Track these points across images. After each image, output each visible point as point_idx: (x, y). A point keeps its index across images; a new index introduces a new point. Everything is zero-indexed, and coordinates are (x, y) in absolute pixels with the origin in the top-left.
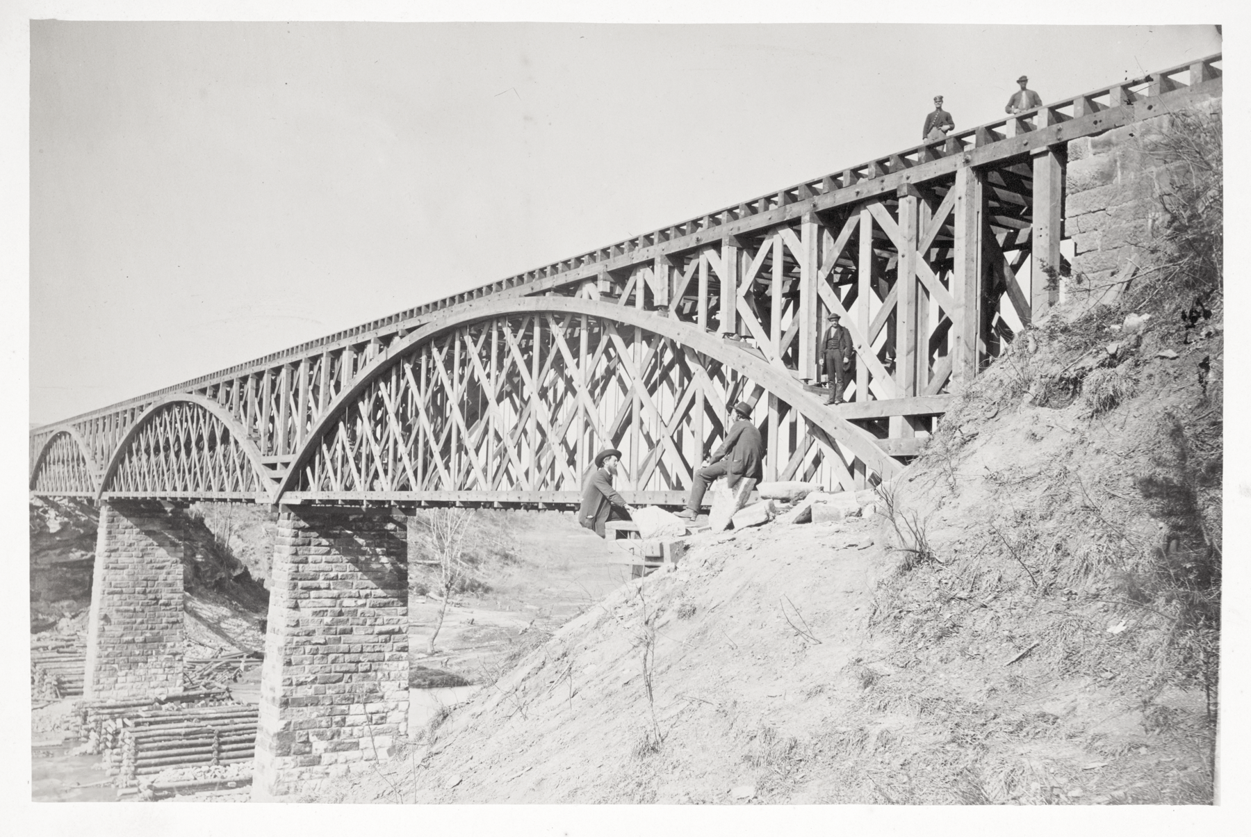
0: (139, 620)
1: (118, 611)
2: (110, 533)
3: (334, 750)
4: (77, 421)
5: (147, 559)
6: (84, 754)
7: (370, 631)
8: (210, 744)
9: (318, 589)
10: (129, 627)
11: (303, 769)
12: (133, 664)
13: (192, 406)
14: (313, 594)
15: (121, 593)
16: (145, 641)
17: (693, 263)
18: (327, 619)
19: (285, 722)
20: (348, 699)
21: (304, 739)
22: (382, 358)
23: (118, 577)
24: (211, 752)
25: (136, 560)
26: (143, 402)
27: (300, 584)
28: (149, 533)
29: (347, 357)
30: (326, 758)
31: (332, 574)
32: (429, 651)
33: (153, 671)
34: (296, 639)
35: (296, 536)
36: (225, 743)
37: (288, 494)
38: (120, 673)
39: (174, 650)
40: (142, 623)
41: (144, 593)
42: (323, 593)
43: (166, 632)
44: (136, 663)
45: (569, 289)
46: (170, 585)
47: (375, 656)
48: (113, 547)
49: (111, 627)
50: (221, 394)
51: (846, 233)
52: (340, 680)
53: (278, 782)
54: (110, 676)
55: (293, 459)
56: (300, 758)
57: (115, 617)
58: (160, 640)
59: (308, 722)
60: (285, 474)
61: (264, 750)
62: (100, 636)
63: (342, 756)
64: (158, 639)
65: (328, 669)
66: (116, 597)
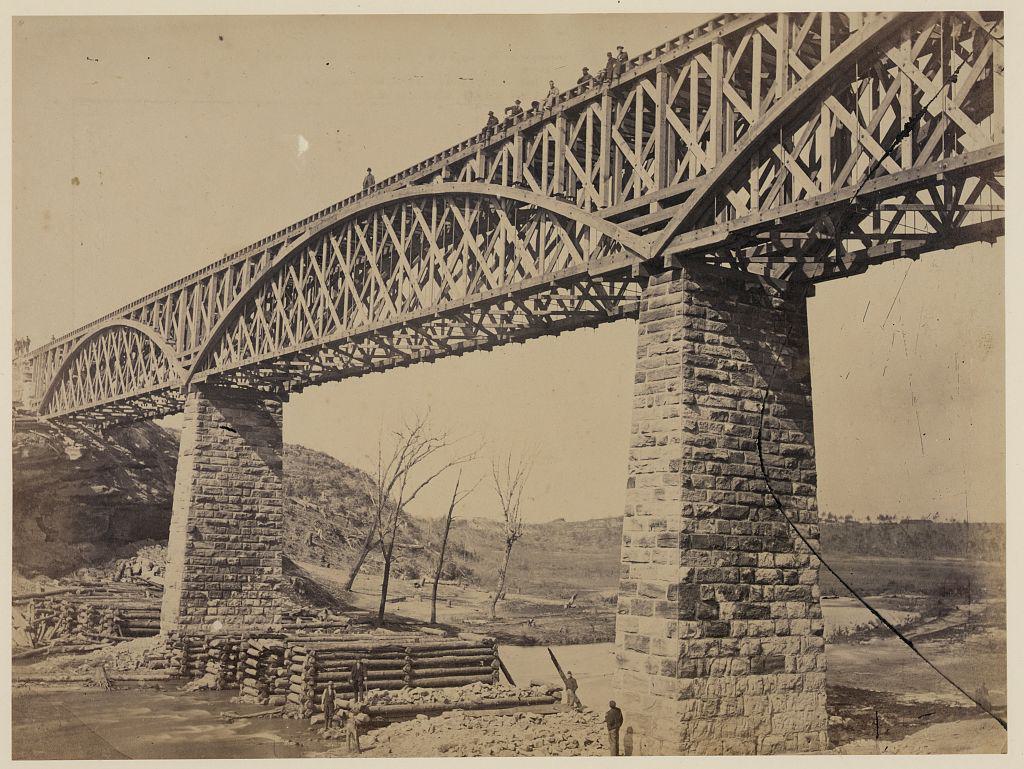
0: (233, 537)
1: (209, 523)
2: (201, 425)
3: (743, 617)
4: (126, 313)
5: (243, 461)
6: (205, 688)
7: (775, 449)
8: (399, 667)
9: (716, 380)
10: (221, 544)
11: (711, 640)
12: (224, 593)
13: (128, 329)
14: (712, 387)
15: (212, 501)
16: (239, 565)
17: (540, 135)
18: (728, 426)
19: (688, 569)
20: (755, 544)
21: (709, 596)
23: (211, 482)
24: (401, 677)
25: (230, 461)
26: (78, 335)
27: (697, 370)
28: (242, 430)
29: (246, 268)
31: (731, 363)
32: (490, 616)
33: (248, 602)
34: (696, 450)
35: (689, 302)
36: (417, 666)
38: (210, 603)
39: (272, 577)
40: (236, 541)
41: (238, 503)
42: (723, 388)
43: (263, 553)
44: (229, 590)
45: (428, 179)
46: (268, 495)
47: (781, 486)
48: (205, 443)
49: (201, 544)
50: (144, 315)
52: (746, 515)
53: (683, 657)
54: (198, 606)
56: (707, 624)
57: (206, 532)
58: (256, 564)
59: (713, 572)
60: (193, 362)
62: (188, 554)
63: (754, 625)
64: (253, 562)
65: (731, 498)
66: (208, 506)
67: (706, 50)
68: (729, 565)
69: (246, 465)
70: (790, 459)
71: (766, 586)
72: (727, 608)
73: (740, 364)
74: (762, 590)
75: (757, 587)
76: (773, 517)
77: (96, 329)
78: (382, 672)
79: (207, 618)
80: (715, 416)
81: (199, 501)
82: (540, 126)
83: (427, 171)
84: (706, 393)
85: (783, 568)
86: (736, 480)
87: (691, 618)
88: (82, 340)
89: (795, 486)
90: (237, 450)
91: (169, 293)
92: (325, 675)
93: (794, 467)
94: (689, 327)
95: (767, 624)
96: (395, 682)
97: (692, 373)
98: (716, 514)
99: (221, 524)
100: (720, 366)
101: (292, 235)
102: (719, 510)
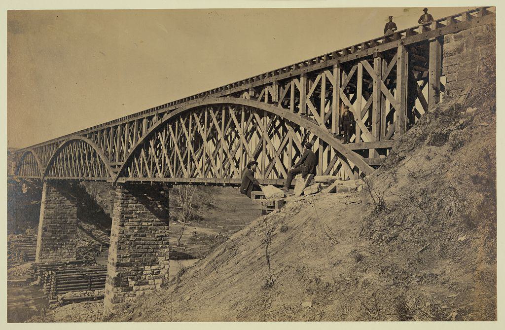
3: (138, 285)
8: (87, 282)
9: (132, 218)
10: (54, 233)
11: (125, 292)
16: (61, 239)
19: (118, 273)
21: (125, 280)
22: (160, 122)
24: (87, 285)
26: (61, 140)
27: (125, 216)
30: (135, 288)
31: (138, 212)
33: (64, 251)
34: (123, 239)
35: (123, 196)
37: (120, 178)
40: (59, 231)
41: (61, 218)
42: (134, 220)
45: (237, 95)
46: (72, 216)
51: (352, 72)
52: (141, 256)
53: (115, 297)
54: (46, 253)
55: (122, 164)
57: (49, 229)
60: (119, 170)
61: (109, 286)
66: (49, 220)
67: (271, 84)
68: (134, 270)
69: (64, 206)
70: (159, 238)
71: (147, 276)
72: (132, 283)
73: (141, 212)
74: (146, 277)
75: (144, 276)
76: (152, 255)
77: (67, 139)
78: (80, 284)
79: (49, 257)
80: (130, 228)
81: (46, 219)
82: (290, 79)
83: (239, 89)
84: (128, 222)
85: (154, 270)
86: (137, 246)
87: (119, 287)
88: (174, 113)
89: (160, 246)
90: (60, 201)
91: (136, 119)
92: (59, 286)
93: (160, 240)
94: (123, 203)
95: (147, 286)
96: (85, 287)
97: (123, 217)
98: (130, 257)
99: (54, 226)
100: (133, 213)
101: (171, 109)
102: (131, 255)
